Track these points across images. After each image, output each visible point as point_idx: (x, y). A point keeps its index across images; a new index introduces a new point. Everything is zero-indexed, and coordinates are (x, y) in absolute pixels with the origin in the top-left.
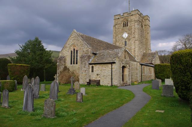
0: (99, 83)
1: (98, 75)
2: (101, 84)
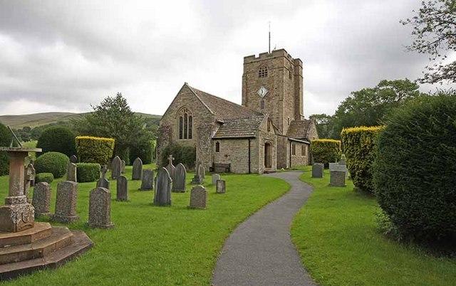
0: (229, 169)
2: (232, 169)
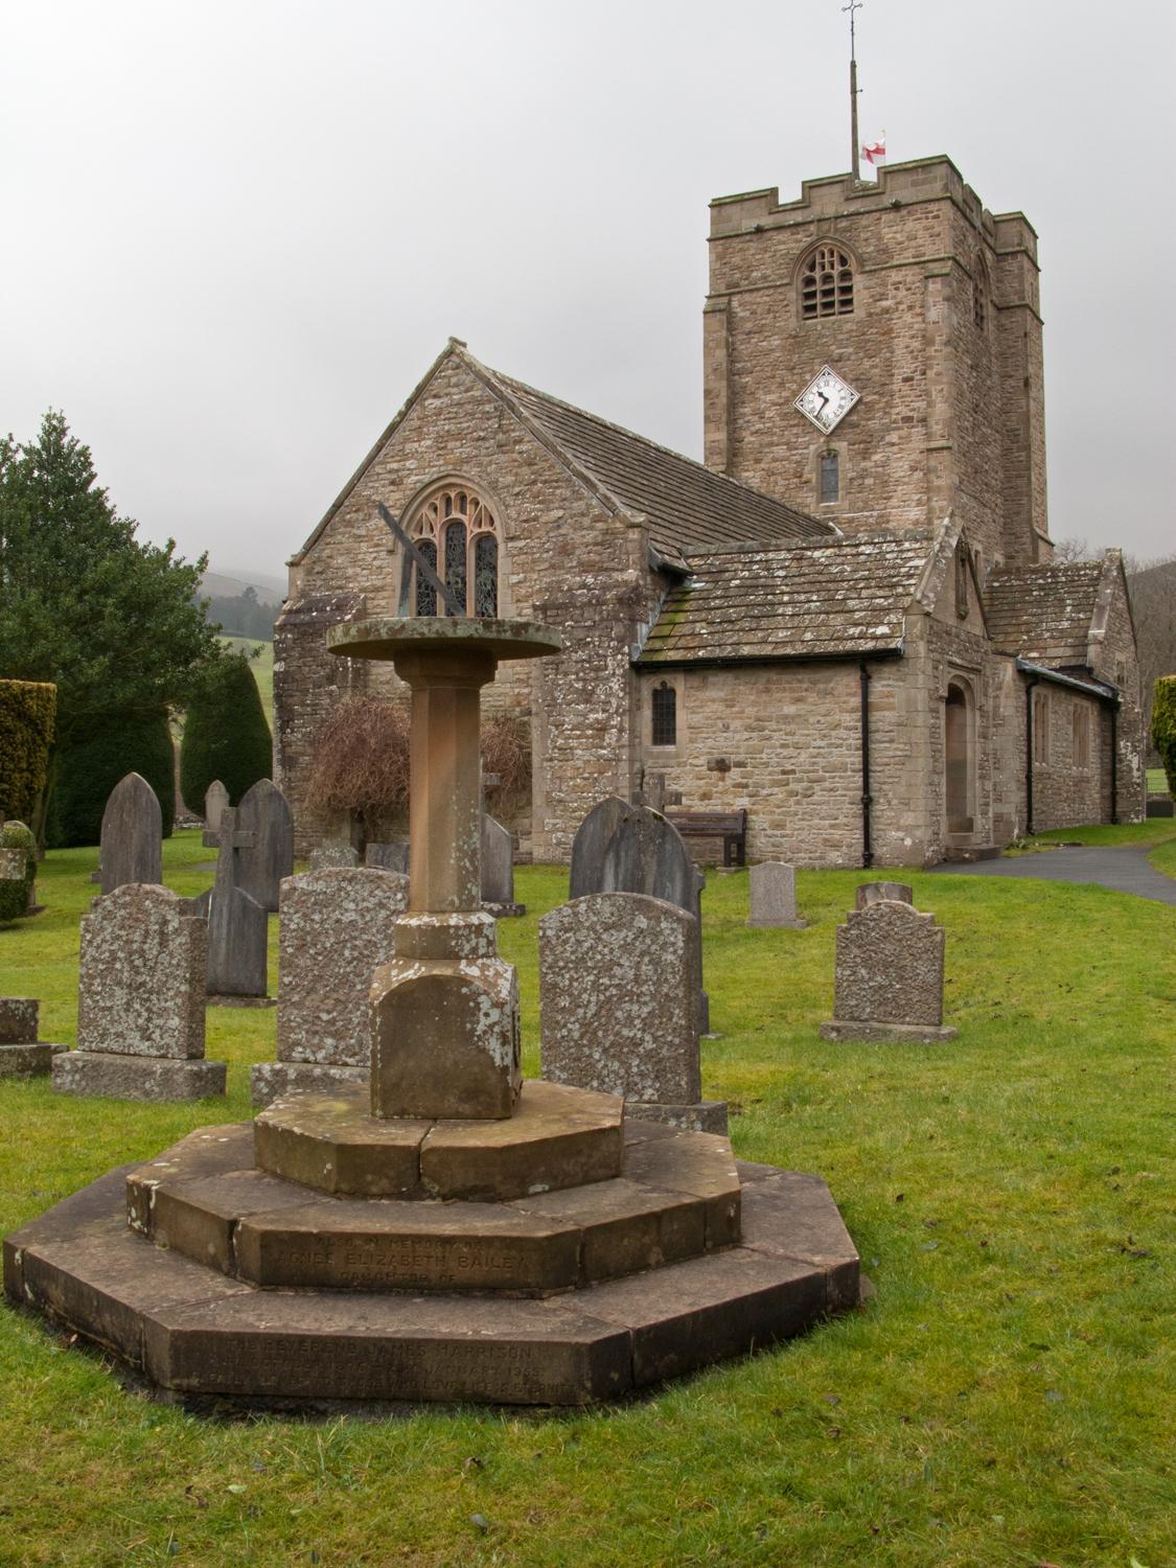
1: (722, 766)
